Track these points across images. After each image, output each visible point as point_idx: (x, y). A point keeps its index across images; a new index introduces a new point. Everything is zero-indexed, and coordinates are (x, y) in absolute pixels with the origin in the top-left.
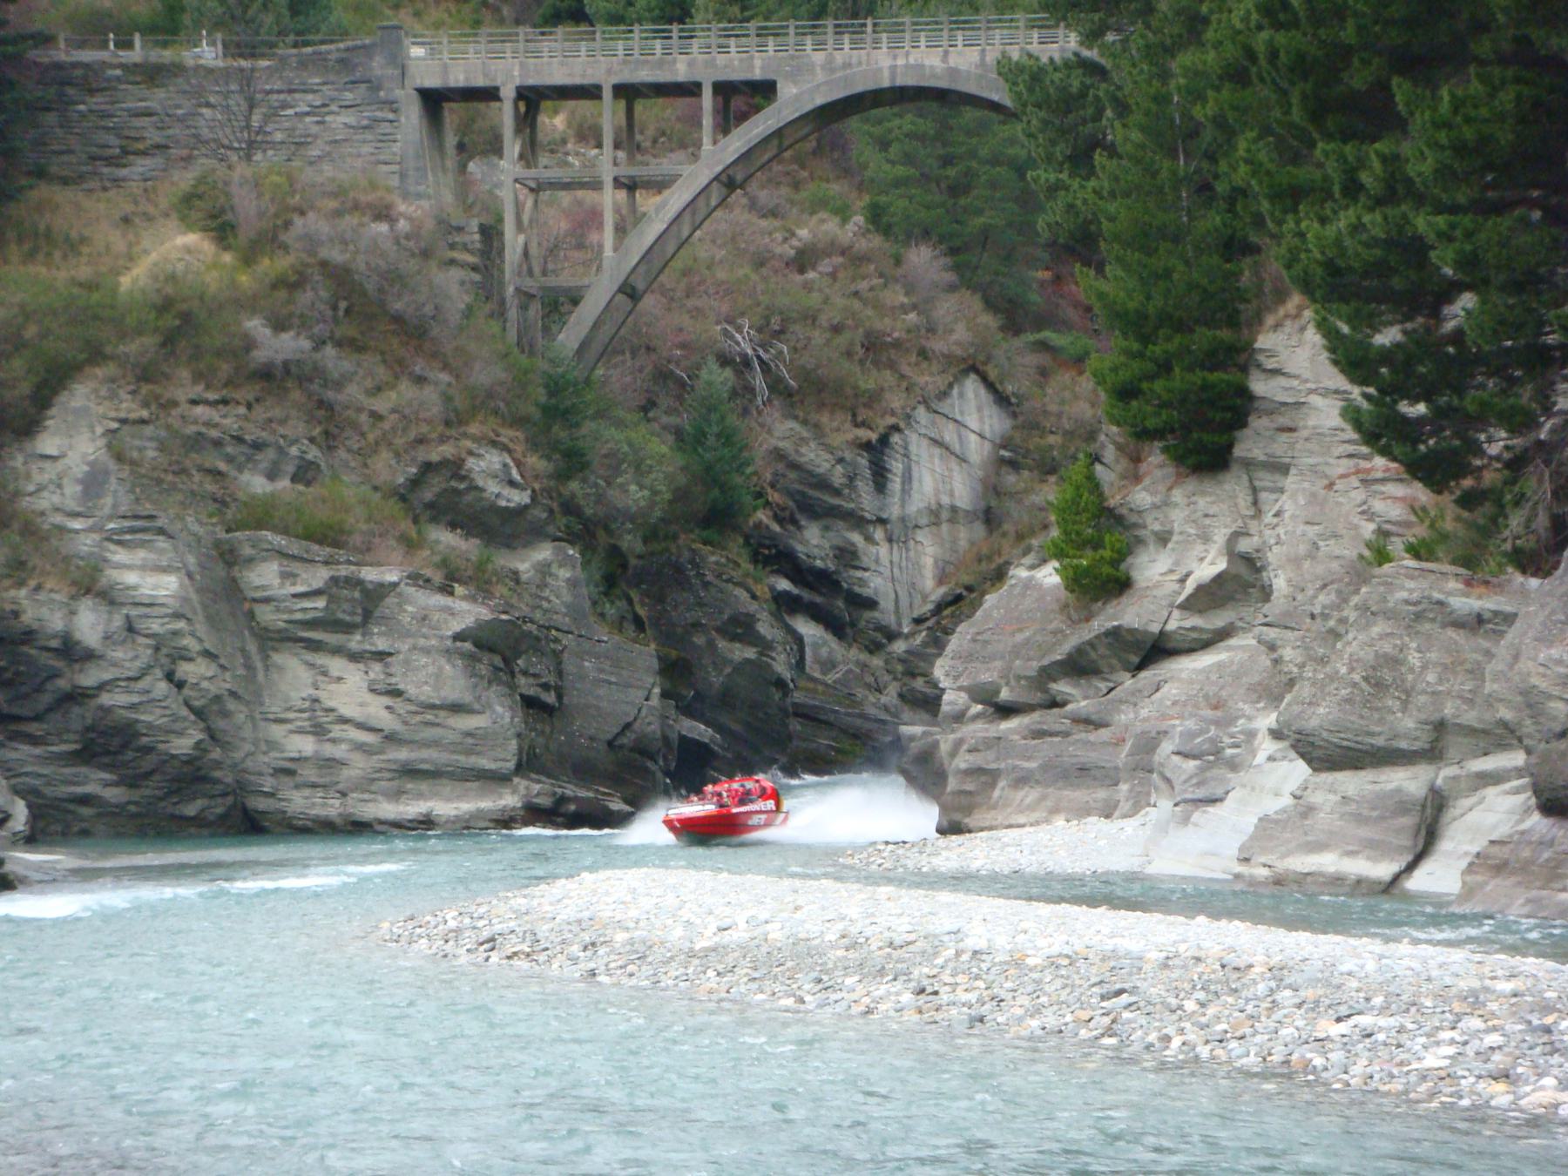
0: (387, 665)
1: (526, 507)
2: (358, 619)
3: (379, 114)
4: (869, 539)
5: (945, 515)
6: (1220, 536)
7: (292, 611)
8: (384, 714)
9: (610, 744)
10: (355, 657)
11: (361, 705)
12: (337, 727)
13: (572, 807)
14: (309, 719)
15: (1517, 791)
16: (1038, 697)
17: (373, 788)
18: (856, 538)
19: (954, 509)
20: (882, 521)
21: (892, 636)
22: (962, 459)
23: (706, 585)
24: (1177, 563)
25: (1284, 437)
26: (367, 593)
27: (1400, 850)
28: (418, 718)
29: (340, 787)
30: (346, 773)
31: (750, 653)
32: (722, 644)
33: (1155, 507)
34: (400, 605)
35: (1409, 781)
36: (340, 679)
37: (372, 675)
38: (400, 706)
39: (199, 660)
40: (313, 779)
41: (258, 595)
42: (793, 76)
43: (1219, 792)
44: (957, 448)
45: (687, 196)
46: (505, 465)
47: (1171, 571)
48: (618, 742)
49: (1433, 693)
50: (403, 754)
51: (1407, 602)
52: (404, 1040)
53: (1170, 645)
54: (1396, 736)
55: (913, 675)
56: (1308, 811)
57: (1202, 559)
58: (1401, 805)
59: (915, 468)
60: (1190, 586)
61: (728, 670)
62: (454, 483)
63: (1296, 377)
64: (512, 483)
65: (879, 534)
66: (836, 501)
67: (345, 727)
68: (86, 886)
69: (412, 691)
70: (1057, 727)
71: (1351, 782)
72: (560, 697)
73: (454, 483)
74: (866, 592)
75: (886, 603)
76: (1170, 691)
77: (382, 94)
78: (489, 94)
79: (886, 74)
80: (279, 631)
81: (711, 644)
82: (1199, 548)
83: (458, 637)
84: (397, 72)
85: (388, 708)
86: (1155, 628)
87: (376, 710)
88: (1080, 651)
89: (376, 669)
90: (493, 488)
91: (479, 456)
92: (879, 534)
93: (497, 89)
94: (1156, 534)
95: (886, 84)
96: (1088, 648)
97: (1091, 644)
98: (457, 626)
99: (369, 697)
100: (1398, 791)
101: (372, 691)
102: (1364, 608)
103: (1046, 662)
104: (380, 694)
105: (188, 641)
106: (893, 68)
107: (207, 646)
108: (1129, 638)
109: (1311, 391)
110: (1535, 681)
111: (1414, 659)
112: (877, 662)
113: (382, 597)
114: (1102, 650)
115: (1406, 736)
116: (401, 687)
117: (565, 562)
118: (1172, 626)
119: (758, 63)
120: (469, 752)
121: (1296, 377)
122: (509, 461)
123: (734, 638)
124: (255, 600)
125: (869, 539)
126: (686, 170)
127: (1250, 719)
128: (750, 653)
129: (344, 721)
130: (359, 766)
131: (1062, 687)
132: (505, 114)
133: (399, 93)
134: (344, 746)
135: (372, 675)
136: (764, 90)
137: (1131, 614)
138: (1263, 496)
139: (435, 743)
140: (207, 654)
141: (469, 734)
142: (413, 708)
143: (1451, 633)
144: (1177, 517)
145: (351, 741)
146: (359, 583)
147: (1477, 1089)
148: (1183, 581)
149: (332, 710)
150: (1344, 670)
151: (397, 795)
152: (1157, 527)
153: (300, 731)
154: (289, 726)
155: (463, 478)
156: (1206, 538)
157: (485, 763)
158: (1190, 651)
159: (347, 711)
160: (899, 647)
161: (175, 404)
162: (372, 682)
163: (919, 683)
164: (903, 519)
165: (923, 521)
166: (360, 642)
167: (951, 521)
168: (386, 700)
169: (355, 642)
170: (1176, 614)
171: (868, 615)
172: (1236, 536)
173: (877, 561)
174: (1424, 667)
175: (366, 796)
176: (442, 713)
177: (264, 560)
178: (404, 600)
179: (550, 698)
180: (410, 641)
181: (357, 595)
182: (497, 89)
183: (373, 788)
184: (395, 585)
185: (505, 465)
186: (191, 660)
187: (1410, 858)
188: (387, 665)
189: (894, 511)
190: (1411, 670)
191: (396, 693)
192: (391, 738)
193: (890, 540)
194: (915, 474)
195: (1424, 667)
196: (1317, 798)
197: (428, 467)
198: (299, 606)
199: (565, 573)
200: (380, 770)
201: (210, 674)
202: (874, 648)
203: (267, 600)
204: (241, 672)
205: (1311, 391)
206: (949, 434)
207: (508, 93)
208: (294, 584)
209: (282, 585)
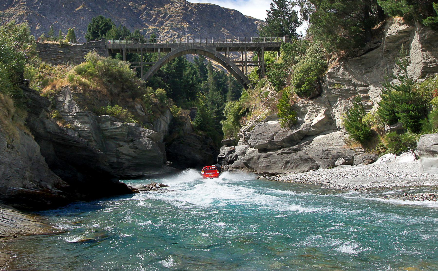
7: (113, 132)
8: (133, 153)
11: (128, 151)
22: (167, 123)
28: (142, 153)
40: (116, 167)
42: (174, 47)
44: (166, 121)
46: (141, 108)
50: (137, 161)
64: (142, 111)
68: (175, 175)
69: (140, 147)
70: (288, 152)
80: (109, 136)
87: (132, 152)
88: (291, 135)
89: (131, 144)
96: (293, 135)
97: (294, 134)
99: (129, 149)
101: (131, 148)
104: (132, 149)
105: (92, 138)
107: (95, 139)
108: (302, 132)
116: (138, 147)
129: (124, 154)
134: (123, 160)
141: (152, 157)
142: (140, 151)
144: (309, 109)
145: (125, 159)
149: (121, 152)
153: (114, 157)
159: (125, 152)
161: (80, 86)
162: (130, 146)
168: (133, 150)
175: (129, 170)
177: (107, 121)
185: (141, 108)
186: (92, 142)
188: (134, 143)
198: (114, 131)
201: (95, 145)
203: (107, 130)
206: (165, 119)
209: (111, 126)
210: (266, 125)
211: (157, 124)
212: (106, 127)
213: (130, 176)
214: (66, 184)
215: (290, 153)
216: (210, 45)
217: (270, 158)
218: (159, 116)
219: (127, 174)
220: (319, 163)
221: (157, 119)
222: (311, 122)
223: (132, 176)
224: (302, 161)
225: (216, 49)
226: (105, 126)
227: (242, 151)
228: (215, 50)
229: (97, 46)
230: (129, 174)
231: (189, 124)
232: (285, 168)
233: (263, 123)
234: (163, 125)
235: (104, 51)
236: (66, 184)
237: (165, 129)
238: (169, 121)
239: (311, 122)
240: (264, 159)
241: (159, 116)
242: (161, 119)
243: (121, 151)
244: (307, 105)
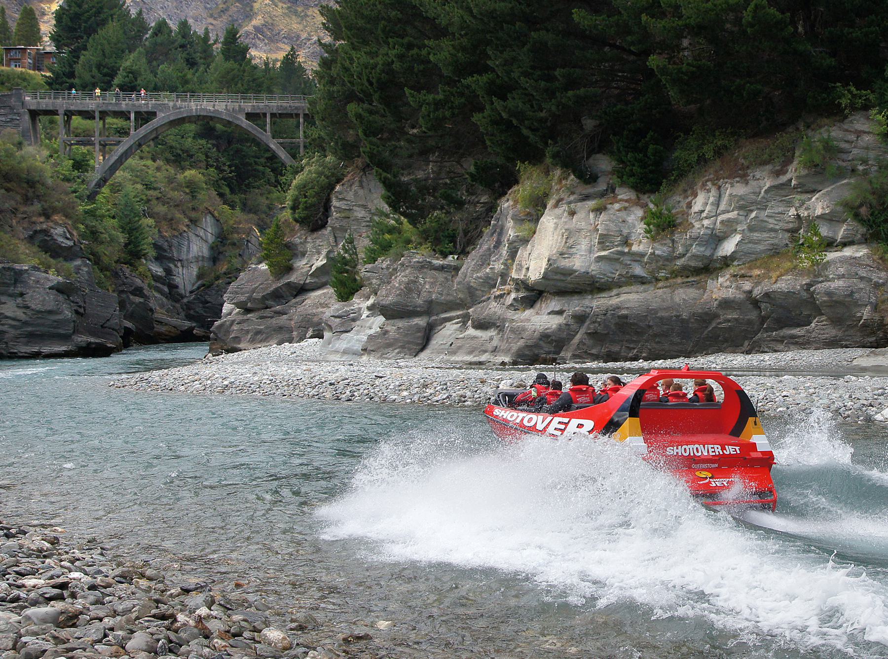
1: (72, 246)
2: (13, 282)
3: (14, 117)
4: (176, 266)
5: (200, 259)
6: (324, 252)
8: (22, 314)
9: (102, 326)
10: (11, 295)
13: (94, 346)
15: (457, 323)
16: (261, 306)
18: (171, 265)
19: (203, 257)
20: (180, 260)
21: (183, 297)
23: (126, 278)
24: (309, 261)
25: (347, 220)
26: (15, 273)
27: (418, 344)
29: (5, 340)
30: (7, 336)
31: (142, 300)
32: (131, 297)
33: (301, 243)
34: (28, 277)
35: (420, 321)
36: (5, 303)
37: (18, 302)
38: (29, 312)
42: (161, 111)
43: (349, 329)
44: (204, 237)
45: (125, 148)
46: (64, 232)
47: (306, 264)
48: (105, 325)
49: (429, 292)
50: (30, 329)
51: (418, 262)
52: (814, 395)
53: (307, 287)
54: (416, 307)
55: (190, 309)
56: (386, 332)
58: (418, 328)
60: (314, 268)
61: (134, 306)
62: (46, 238)
63: (349, 201)
64: (68, 239)
65: (179, 264)
66: (165, 254)
69: (33, 306)
70: (269, 315)
71: (401, 323)
72: (85, 310)
73: (46, 238)
74: (176, 283)
75: (181, 286)
76: (308, 302)
78: (54, 113)
81: (128, 297)
83: (50, 288)
85: (24, 313)
86: (302, 282)
87: (20, 314)
88: (276, 289)
89: (19, 300)
90: (60, 239)
91: (56, 229)
92: (179, 264)
93: (57, 111)
94: (301, 252)
95: (194, 114)
97: (280, 287)
98: (50, 284)
99: (16, 309)
100: (417, 324)
101: (18, 307)
102: (402, 265)
103: (264, 294)
106: (196, 109)
109: (353, 206)
110: (472, 284)
111: (421, 281)
112: (178, 305)
113: (22, 275)
114: (284, 289)
115: (420, 306)
117: (86, 265)
118: (308, 281)
119: (150, 106)
120: (55, 328)
121: (349, 201)
123: (136, 295)
125: (176, 266)
126: (125, 139)
127: (359, 304)
128: (142, 300)
129: (7, 317)
130: (13, 332)
131: (270, 303)
132: (59, 119)
136: (152, 115)
137: (293, 278)
138: (338, 239)
139: (43, 325)
141: (55, 321)
143: (433, 272)
144: (309, 246)
145: (9, 324)
146: (14, 269)
148: (311, 267)
150: (397, 285)
151: (26, 344)
152: (302, 250)
155: (49, 236)
156: (319, 253)
157: (61, 331)
158: (313, 290)
159: (9, 314)
160: (185, 300)
162: (19, 304)
163: (192, 312)
164: (187, 260)
167: (202, 261)
169: (11, 290)
170: (309, 278)
171: (175, 290)
172: (329, 252)
173: (178, 273)
174: (425, 283)
175: (15, 344)
176: (45, 314)
178: (30, 275)
179: (82, 310)
180: (33, 289)
181: (12, 273)
182: (57, 111)
184: (27, 270)
185: (64, 232)
187: (420, 347)
189: (184, 257)
190: (420, 284)
191: (27, 307)
192: (26, 323)
193: (183, 267)
195: (425, 283)
196: (388, 328)
197: (36, 232)
199: (86, 269)
200: (20, 334)
202: (177, 301)
205: (353, 206)
206: (202, 233)
207: (61, 112)
211: (180, 245)
213: (15, 353)
214: (720, 323)
215: (272, 317)
216: (233, 109)
218: (185, 229)
219: (12, 351)
221: (181, 234)
223: (21, 355)
225: (244, 115)
228: (243, 118)
229: (6, 105)
230: (16, 351)
231: (257, 244)
232: (252, 341)
233: (254, 266)
234: (195, 247)
235: (18, 114)
236: (720, 323)
237: (200, 254)
238: (211, 239)
241: (185, 229)
242: (190, 234)
244: (305, 242)
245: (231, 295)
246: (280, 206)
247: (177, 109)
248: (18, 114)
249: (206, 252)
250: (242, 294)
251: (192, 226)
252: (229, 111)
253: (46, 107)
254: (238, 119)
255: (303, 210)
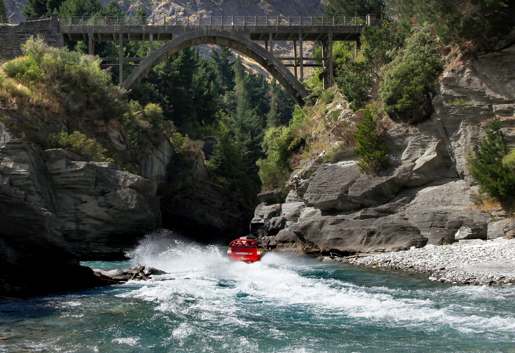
0: (106, 197)
3: (51, 40)
7: (69, 178)
8: (104, 214)
12: (85, 219)
14: (74, 216)
17: (99, 241)
19: (162, 176)
26: (97, 171)
28: (119, 215)
29: (87, 240)
30: (89, 236)
37: (100, 200)
38: (111, 210)
39: (36, 195)
41: (55, 172)
42: (176, 32)
44: (162, 159)
46: (119, 136)
57: (422, 154)
59: (154, 164)
64: (121, 142)
67: (89, 219)
69: (117, 205)
70: (373, 214)
77: (52, 34)
79: (205, 32)
80: (63, 185)
82: (420, 150)
84: (56, 28)
85: (106, 212)
87: (102, 212)
88: (379, 187)
89: (101, 199)
97: (383, 184)
99: (98, 208)
101: (100, 206)
104: (103, 207)
105: (32, 188)
107: (39, 190)
122: (120, 134)
124: (54, 174)
129: (89, 217)
133: (57, 34)
134: (88, 226)
135: (100, 200)
140: (38, 192)
141: (138, 221)
142: (117, 212)
147: (483, 318)
153: (71, 221)
154: (66, 219)
159: (89, 213)
162: (101, 202)
165: (155, 179)
166: (93, 189)
177: (60, 159)
181: (95, 171)
183: (99, 241)
186: (33, 194)
191: (111, 207)
194: (154, 166)
198: (72, 176)
201: (39, 200)
203: (59, 174)
204: (49, 199)
206: (161, 156)
208: (71, 167)
209: (67, 167)
210: (334, 168)
211: (146, 165)
212: (58, 169)
216: (240, 30)
217: (342, 225)
220: (426, 234)
221: (147, 156)
222: (413, 164)
224: (396, 231)
225: (249, 36)
226: (55, 167)
227: (292, 214)
228: (247, 37)
230: (97, 251)
233: (330, 165)
235: (55, 37)
237: (160, 173)
238: (167, 160)
239: (413, 164)
240: (331, 226)
241: (151, 151)
243: (84, 211)
245: (315, 194)
246: (205, 137)
247: (190, 30)
248: (55, 37)
249: (163, 172)
250: (330, 192)
251: (155, 150)
252: (236, 32)
253: (78, 30)
254: (244, 39)
255: (408, 99)
